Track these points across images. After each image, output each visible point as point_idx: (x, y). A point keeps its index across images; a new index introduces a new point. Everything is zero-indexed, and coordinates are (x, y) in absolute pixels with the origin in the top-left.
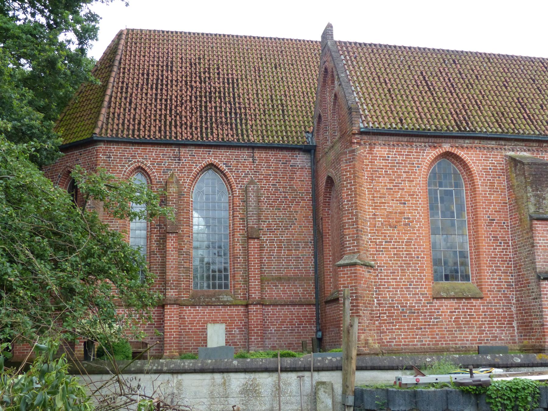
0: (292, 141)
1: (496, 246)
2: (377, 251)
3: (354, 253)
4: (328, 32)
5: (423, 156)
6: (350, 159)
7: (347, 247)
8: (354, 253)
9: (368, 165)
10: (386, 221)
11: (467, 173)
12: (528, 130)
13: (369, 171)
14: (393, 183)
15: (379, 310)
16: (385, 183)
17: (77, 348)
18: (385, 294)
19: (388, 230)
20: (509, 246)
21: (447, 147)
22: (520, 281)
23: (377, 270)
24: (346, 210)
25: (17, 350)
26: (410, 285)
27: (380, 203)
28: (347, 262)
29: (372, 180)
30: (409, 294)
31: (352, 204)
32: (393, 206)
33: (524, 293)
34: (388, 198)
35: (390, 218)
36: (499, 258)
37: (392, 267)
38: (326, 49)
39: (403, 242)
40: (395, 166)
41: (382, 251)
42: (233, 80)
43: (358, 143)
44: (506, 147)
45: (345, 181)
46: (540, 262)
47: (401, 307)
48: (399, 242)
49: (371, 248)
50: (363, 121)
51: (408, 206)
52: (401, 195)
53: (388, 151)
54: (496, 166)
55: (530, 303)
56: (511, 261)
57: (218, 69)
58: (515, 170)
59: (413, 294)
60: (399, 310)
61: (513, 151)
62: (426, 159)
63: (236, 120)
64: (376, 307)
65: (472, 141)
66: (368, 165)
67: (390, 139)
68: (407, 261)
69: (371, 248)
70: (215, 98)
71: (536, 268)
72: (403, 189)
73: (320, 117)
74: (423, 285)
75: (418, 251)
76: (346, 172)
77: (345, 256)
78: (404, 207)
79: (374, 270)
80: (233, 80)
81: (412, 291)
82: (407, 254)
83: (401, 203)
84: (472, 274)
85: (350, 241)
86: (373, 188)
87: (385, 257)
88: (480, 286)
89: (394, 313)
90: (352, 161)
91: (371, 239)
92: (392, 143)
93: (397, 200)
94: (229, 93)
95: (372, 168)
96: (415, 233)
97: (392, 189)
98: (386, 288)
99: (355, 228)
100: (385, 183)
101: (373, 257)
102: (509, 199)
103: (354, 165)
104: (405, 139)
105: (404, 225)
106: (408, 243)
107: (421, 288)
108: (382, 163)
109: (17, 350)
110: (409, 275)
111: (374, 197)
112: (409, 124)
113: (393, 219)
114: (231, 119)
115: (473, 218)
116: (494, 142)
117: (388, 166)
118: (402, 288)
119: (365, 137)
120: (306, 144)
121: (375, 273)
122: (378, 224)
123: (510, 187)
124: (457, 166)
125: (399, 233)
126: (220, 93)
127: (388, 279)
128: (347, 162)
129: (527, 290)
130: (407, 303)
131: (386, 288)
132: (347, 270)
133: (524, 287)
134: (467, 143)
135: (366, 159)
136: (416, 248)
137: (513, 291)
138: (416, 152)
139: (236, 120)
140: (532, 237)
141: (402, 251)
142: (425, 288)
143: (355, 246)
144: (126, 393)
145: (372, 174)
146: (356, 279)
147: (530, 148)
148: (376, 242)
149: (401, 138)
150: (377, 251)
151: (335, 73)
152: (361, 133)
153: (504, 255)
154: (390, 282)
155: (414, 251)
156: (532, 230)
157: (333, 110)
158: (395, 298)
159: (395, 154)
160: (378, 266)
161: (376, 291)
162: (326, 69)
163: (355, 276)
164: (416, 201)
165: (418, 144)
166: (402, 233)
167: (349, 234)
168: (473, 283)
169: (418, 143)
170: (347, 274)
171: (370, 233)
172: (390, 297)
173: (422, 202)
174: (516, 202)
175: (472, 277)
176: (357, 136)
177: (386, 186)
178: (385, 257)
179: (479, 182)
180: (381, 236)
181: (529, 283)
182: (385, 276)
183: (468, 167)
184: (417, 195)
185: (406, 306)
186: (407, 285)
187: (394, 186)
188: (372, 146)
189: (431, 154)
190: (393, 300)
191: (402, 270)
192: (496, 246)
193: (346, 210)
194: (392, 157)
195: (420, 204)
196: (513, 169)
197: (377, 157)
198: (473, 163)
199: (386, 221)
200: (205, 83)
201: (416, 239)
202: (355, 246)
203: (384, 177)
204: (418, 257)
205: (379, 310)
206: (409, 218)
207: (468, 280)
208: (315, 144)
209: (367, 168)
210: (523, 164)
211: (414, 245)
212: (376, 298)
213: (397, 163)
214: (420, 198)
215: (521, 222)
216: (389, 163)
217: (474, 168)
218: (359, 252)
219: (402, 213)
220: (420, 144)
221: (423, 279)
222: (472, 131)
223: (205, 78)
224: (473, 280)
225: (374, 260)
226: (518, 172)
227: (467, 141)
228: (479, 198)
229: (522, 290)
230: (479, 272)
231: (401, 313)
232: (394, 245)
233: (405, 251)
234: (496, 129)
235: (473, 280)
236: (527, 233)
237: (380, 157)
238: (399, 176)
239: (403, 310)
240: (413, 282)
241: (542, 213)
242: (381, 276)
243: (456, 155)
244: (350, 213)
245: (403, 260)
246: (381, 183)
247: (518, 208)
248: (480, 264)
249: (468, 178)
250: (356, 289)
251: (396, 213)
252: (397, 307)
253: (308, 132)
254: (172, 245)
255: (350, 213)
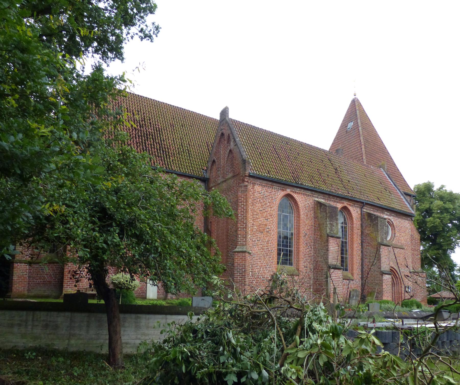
0: (196, 174)
1: (307, 248)
2: (253, 245)
3: (243, 245)
4: (224, 113)
5: (277, 194)
6: (244, 190)
7: (239, 241)
8: (243, 245)
9: (251, 195)
10: (258, 229)
11: (296, 207)
12: (324, 188)
13: (252, 199)
14: (262, 207)
15: (252, 279)
16: (259, 207)
17: (65, 289)
18: (255, 270)
19: (259, 234)
20: (312, 249)
21: (288, 191)
22: (317, 268)
23: (252, 256)
24: (240, 220)
25: (15, 288)
26: (267, 266)
27: (256, 218)
28: (240, 250)
29: (253, 204)
30: (266, 271)
31: (243, 217)
32: (261, 220)
33: (319, 275)
34: (260, 215)
35: (260, 227)
36: (308, 255)
37: (259, 255)
38: (224, 122)
39: (265, 241)
40: (264, 198)
41: (255, 245)
42: (159, 129)
43: (247, 181)
44: (315, 195)
45: (240, 203)
46: (330, 259)
47: (262, 277)
48: (263, 241)
49: (250, 243)
50: (251, 169)
51: (269, 222)
52: (266, 215)
53: (262, 189)
54: (310, 205)
55: (322, 280)
56: (312, 257)
57: (150, 120)
58: (320, 208)
59: (268, 271)
60: (261, 279)
61: (317, 198)
62: (279, 196)
63: (163, 155)
64: (251, 277)
65: (300, 190)
66: (251, 195)
67: (263, 182)
68: (266, 252)
69: (250, 243)
70: (150, 139)
71: (328, 262)
72: (267, 212)
73: (214, 161)
74: (273, 266)
75: (272, 247)
76: (241, 198)
77: (238, 247)
78: (267, 222)
79: (251, 256)
80: (159, 129)
81: (268, 269)
82: (267, 248)
83: (266, 220)
84: (294, 262)
85: (241, 238)
86: (253, 209)
87: (256, 249)
88: (352, 274)
89: (259, 281)
90: (245, 192)
91: (250, 238)
92: (263, 185)
93: (264, 218)
94: (158, 137)
95: (253, 197)
96: (271, 237)
97: (262, 211)
98: (256, 266)
99: (244, 231)
100: (259, 207)
101: (251, 248)
102: (314, 224)
103: (247, 194)
104: (270, 183)
105: (266, 232)
106: (268, 243)
107: (272, 268)
108: (258, 195)
109: (15, 288)
110: (267, 260)
111: (253, 214)
112: (273, 175)
113: (261, 228)
114: (160, 154)
115: (297, 232)
116: (310, 192)
117: (261, 197)
118: (263, 267)
119: (251, 179)
120: (203, 176)
121: (251, 257)
122: (255, 230)
123: (316, 217)
124: (291, 202)
125: (264, 236)
126: (152, 136)
127: (257, 261)
128: (242, 192)
129: (321, 273)
130: (265, 276)
131: (256, 266)
132: (240, 255)
133: (319, 271)
134: (298, 190)
135: (251, 192)
136: (271, 245)
137: (312, 273)
138: (274, 192)
139: (163, 155)
140: (328, 246)
141: (264, 246)
142: (274, 268)
143: (244, 241)
144: (177, 330)
145: (253, 201)
146: (245, 260)
147: (325, 198)
148: (253, 240)
149: (268, 183)
150: (253, 245)
151: (231, 137)
152: (250, 176)
153: (310, 253)
154: (258, 263)
155: (270, 247)
156: (328, 242)
157: (227, 159)
158: (259, 272)
159: (265, 191)
160: (253, 254)
161: (251, 268)
162: (223, 134)
163: (244, 259)
164: (273, 219)
165: (276, 187)
166: (265, 236)
167: (241, 234)
168: (349, 272)
169: (276, 186)
170: (240, 257)
171: (250, 234)
172: (257, 272)
173: (275, 220)
174: (319, 226)
175: (294, 264)
176: (247, 177)
177: (259, 208)
178: (256, 249)
179: (302, 213)
180: (255, 237)
181: (323, 269)
182: (256, 259)
183: (297, 203)
184: (273, 216)
185: (264, 277)
186: (265, 266)
187: (263, 209)
188: (254, 184)
189: (282, 193)
190: (258, 274)
191: (264, 257)
192: (307, 248)
193: (240, 220)
194: (263, 193)
195: (275, 221)
196: (319, 208)
197: (256, 191)
198: (300, 202)
199: (258, 229)
200: (143, 128)
201: (271, 241)
202: (244, 241)
203: (258, 203)
204: (272, 251)
205: (252, 279)
206: (269, 229)
207: (292, 265)
208: (208, 177)
209: (251, 197)
210: (326, 206)
211: (270, 244)
212: (251, 271)
213: (265, 196)
214: (275, 218)
215: (321, 237)
216: (261, 196)
217: (301, 205)
218: (246, 245)
219: (266, 225)
220: (276, 187)
221: (273, 263)
222: (301, 184)
223: (143, 124)
224: (294, 265)
225: (251, 250)
226: (322, 210)
227: (298, 189)
228: (301, 221)
229: (318, 273)
230: (298, 261)
231: (262, 281)
232: (261, 243)
233: (266, 247)
234: (310, 185)
235: (294, 265)
236: (324, 243)
237: (258, 191)
238: (266, 204)
239: (263, 279)
240: (268, 264)
241: (333, 234)
242: (254, 259)
243: (292, 196)
244: (242, 222)
245: (265, 252)
246: (257, 206)
247: (320, 229)
248: (299, 257)
249: (296, 210)
250: (245, 266)
251: (263, 225)
252: (261, 277)
253: (203, 169)
254: (274, 241)
255: (242, 222)
